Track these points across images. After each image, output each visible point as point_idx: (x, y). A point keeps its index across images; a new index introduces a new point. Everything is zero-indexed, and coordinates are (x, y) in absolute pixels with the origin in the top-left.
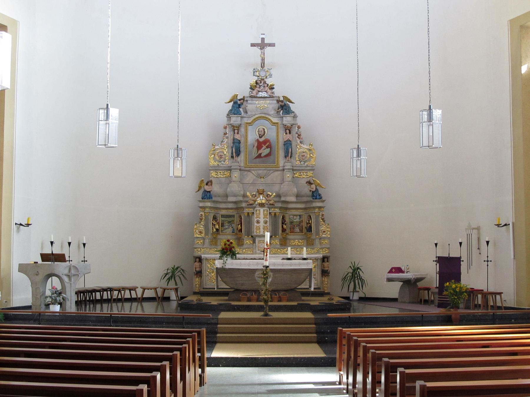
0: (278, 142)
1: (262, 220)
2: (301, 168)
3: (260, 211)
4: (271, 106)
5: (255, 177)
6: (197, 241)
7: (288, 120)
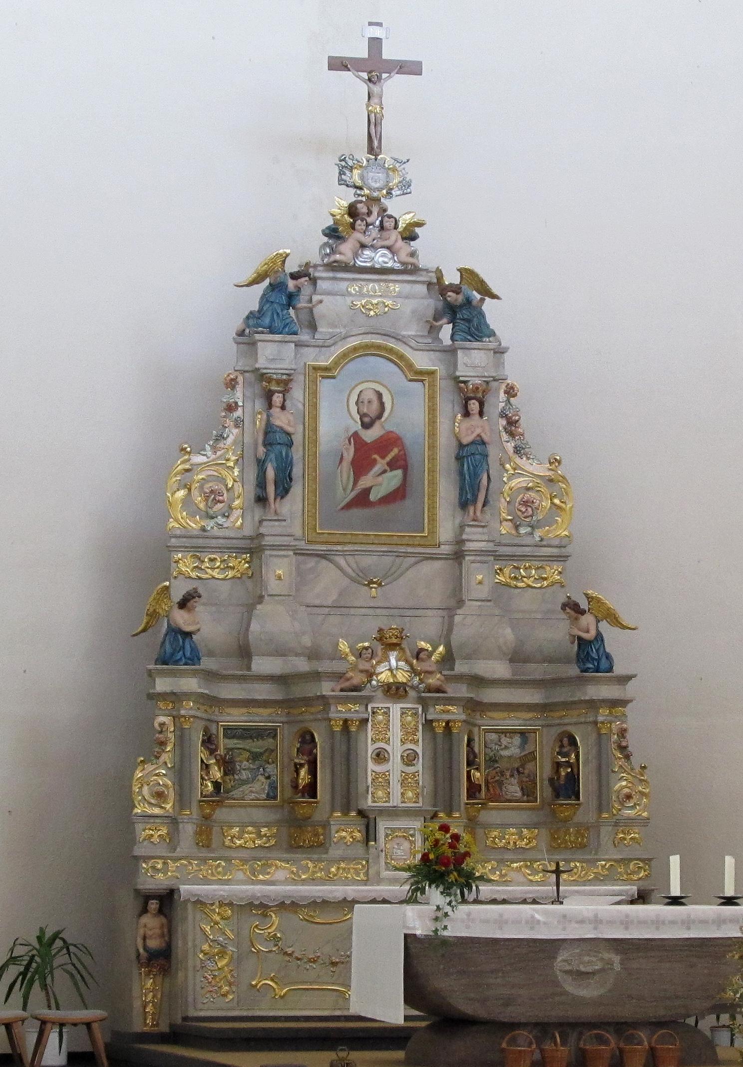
0: (432, 447)
1: (396, 749)
2: (519, 551)
3: (387, 714)
4: (403, 305)
5: (347, 581)
6: (143, 832)
7: (473, 362)
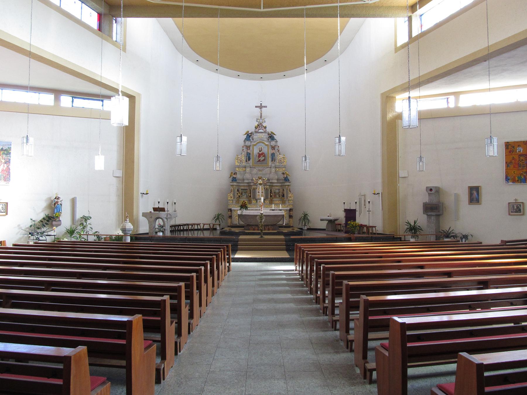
1: (260, 191)
4: (265, 136)
7: (273, 143)
